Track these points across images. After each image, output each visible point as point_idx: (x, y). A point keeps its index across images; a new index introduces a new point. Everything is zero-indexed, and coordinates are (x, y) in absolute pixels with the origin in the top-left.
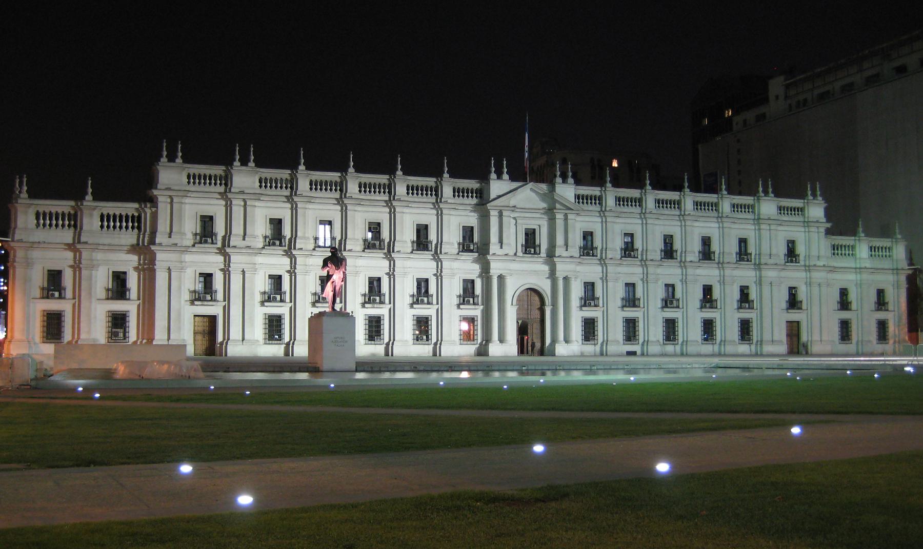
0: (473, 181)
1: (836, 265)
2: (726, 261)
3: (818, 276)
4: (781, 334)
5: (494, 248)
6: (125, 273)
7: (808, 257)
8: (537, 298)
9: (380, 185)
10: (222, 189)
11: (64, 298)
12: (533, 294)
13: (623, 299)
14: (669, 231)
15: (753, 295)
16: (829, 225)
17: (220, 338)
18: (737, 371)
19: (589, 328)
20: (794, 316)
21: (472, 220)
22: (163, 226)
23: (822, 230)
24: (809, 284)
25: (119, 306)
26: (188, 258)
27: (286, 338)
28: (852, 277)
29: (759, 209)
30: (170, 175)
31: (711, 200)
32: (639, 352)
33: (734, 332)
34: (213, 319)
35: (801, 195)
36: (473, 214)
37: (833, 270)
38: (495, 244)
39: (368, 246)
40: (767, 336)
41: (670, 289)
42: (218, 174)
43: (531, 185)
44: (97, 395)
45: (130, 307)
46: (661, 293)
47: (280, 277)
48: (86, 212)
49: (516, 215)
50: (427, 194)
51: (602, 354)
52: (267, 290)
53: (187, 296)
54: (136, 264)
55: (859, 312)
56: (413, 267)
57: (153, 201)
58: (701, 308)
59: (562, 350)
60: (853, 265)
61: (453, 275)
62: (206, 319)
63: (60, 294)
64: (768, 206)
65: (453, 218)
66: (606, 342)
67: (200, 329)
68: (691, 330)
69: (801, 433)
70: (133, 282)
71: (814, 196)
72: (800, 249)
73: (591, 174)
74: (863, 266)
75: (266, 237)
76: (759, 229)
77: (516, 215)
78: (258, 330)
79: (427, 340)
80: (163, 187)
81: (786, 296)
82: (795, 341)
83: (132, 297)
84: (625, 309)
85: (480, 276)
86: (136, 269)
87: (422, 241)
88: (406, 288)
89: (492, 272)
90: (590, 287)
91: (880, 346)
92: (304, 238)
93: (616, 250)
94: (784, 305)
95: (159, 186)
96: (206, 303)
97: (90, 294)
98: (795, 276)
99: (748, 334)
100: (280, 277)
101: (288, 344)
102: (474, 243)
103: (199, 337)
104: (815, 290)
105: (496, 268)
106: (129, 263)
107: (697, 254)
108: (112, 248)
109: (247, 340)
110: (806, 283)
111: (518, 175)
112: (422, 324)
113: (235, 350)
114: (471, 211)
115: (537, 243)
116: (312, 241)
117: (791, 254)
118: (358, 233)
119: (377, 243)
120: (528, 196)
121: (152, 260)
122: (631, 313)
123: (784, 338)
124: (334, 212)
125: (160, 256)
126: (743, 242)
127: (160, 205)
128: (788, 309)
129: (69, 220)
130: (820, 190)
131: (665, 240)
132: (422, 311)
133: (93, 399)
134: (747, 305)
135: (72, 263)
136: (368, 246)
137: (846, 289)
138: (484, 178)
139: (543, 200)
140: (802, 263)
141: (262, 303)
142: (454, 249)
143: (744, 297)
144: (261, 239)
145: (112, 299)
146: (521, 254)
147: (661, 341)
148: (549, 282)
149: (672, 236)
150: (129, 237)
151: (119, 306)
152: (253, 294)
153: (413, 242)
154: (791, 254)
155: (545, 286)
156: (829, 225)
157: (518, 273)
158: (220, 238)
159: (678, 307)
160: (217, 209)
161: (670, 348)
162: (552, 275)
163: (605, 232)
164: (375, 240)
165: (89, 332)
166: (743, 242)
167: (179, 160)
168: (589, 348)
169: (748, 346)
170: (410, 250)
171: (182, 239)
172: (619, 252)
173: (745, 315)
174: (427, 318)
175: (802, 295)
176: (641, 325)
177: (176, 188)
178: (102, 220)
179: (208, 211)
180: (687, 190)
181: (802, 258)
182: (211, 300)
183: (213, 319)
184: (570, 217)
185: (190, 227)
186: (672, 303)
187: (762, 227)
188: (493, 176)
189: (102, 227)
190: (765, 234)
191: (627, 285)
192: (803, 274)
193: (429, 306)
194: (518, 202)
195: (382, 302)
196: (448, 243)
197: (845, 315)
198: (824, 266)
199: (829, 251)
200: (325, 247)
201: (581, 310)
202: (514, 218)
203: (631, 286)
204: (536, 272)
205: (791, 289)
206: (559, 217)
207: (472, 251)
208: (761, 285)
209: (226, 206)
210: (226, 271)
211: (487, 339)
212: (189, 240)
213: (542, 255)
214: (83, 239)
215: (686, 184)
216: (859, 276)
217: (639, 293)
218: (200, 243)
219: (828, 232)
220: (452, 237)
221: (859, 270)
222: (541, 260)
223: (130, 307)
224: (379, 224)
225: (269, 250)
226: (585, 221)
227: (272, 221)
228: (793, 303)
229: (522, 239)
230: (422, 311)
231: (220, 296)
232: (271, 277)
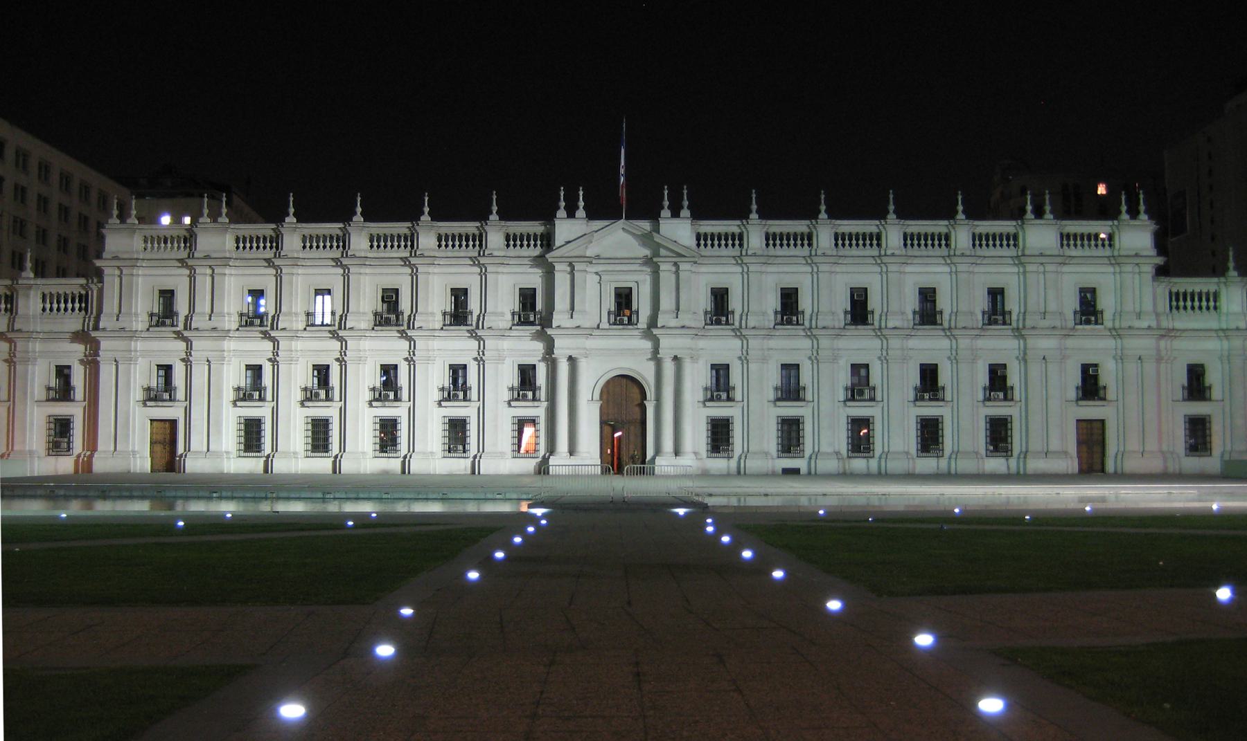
0: (537, 223)
1: (1178, 325)
2: (820, 324)
3: (1140, 345)
5: (559, 318)
6: (69, 367)
7: (1119, 314)
8: (636, 390)
9: (399, 236)
10: (337, 254)
11: (733, 400)
12: (630, 383)
13: (776, 389)
14: (859, 281)
15: (1014, 379)
16: (1160, 261)
17: (180, 449)
19: (720, 434)
20: (1092, 411)
21: (534, 279)
22: (110, 305)
23: (1148, 269)
24: (1121, 358)
25: (62, 409)
26: (139, 345)
27: (267, 448)
28: (1213, 345)
29: (1024, 240)
30: (119, 241)
31: (936, 230)
32: (804, 470)
34: (173, 423)
35: (1018, 214)
36: (644, 268)
37: (1169, 333)
38: (561, 312)
39: (381, 321)
40: (1036, 444)
41: (793, 373)
42: (470, 233)
43: (621, 223)
44: (351, 523)
45: (75, 411)
46: (773, 377)
47: (260, 367)
48: (21, 293)
49: (600, 268)
50: (1082, 246)
52: (243, 385)
53: (139, 395)
54: (81, 356)
55: (1227, 402)
56: (441, 350)
57: (99, 274)
58: (916, 400)
59: (665, 464)
60: (1215, 325)
61: (500, 359)
62: (167, 425)
63: (396, 395)
64: (1041, 235)
65: (503, 279)
66: (746, 454)
67: (160, 437)
68: (827, 433)
69: (1231, 600)
70: (78, 379)
71: (1134, 214)
72: (1106, 302)
73: (716, 200)
74: (1233, 326)
75: (151, 315)
76: (1025, 272)
77: (600, 268)
78: (229, 437)
79: (464, 452)
80: (109, 256)
83: (1213, 397)
84: (778, 403)
85: (544, 359)
86: (82, 362)
87: (459, 315)
88: (433, 378)
89: (557, 352)
90: (721, 372)
91: (52, 460)
92: (290, 314)
93: (764, 314)
95: (105, 255)
96: (160, 404)
97: (25, 393)
98: (1093, 346)
99: (1005, 440)
100: (260, 367)
101: (336, 457)
102: (532, 311)
103: (158, 448)
104: (1035, 370)
105: (563, 347)
106: (73, 354)
107: (911, 316)
108: (52, 336)
109: (215, 449)
110: (1114, 358)
111: (603, 209)
112: (457, 429)
113: (194, 465)
114: (532, 266)
115: (634, 307)
116: (304, 318)
117: (1088, 309)
118: (367, 302)
119: (393, 317)
120: (619, 238)
121: (96, 353)
122: (790, 410)
123: (1072, 448)
124: (333, 278)
125: (104, 345)
126: (996, 294)
127: (106, 279)
128: (1078, 400)
129: (80, 302)
130: (1051, 204)
132: (456, 410)
133: (345, 527)
134: (1001, 395)
135: (7, 356)
136: (381, 321)
138: (548, 217)
139: (644, 245)
140: (1108, 324)
141: (234, 403)
142: (506, 320)
143: (998, 380)
144: (236, 318)
145: (54, 400)
146: (607, 326)
147: (844, 452)
148: (652, 365)
150: (74, 322)
151: (62, 409)
152: (220, 391)
153: (846, 312)
154: (1088, 309)
155: (645, 372)
156: (1160, 261)
157: (598, 356)
158: (181, 319)
159: (872, 399)
160: (178, 281)
161: (859, 464)
162: (656, 357)
163: (746, 286)
164: (390, 312)
165: (24, 442)
166: (996, 294)
167: (1049, 216)
168: (719, 464)
169: (1002, 461)
170: (438, 325)
171: (291, 322)
172: (772, 317)
173: (999, 410)
174: (259, 420)
175: (1107, 376)
176: (808, 428)
177: (125, 256)
179: (168, 284)
180: (892, 216)
181: (1107, 316)
182: (170, 400)
183: (173, 423)
184: (683, 267)
185: (143, 304)
186: (861, 393)
187: (1029, 268)
188: (562, 213)
190: (203, 283)
191: (784, 366)
192: (1111, 343)
194: (597, 249)
195: (397, 399)
196: (494, 314)
197: (1198, 408)
198: (1149, 328)
199: (1163, 304)
200: (322, 325)
201: (145, 405)
202: (597, 273)
203: (791, 370)
204: (632, 352)
205: (1085, 368)
206: (666, 268)
207: (532, 324)
208: (1025, 361)
209: (190, 276)
210: (187, 361)
211: (551, 449)
212: (141, 323)
213: (639, 326)
214: (17, 327)
215: (892, 208)
216: (1226, 344)
217: (806, 378)
218: (157, 326)
219: (1162, 272)
220: (503, 302)
221: (1224, 333)
222: (636, 333)
223: (75, 411)
224: (396, 291)
225: (244, 332)
226: (718, 270)
228: (1090, 386)
229: (610, 303)
230: (456, 410)
231: (542, 394)
232: (248, 367)
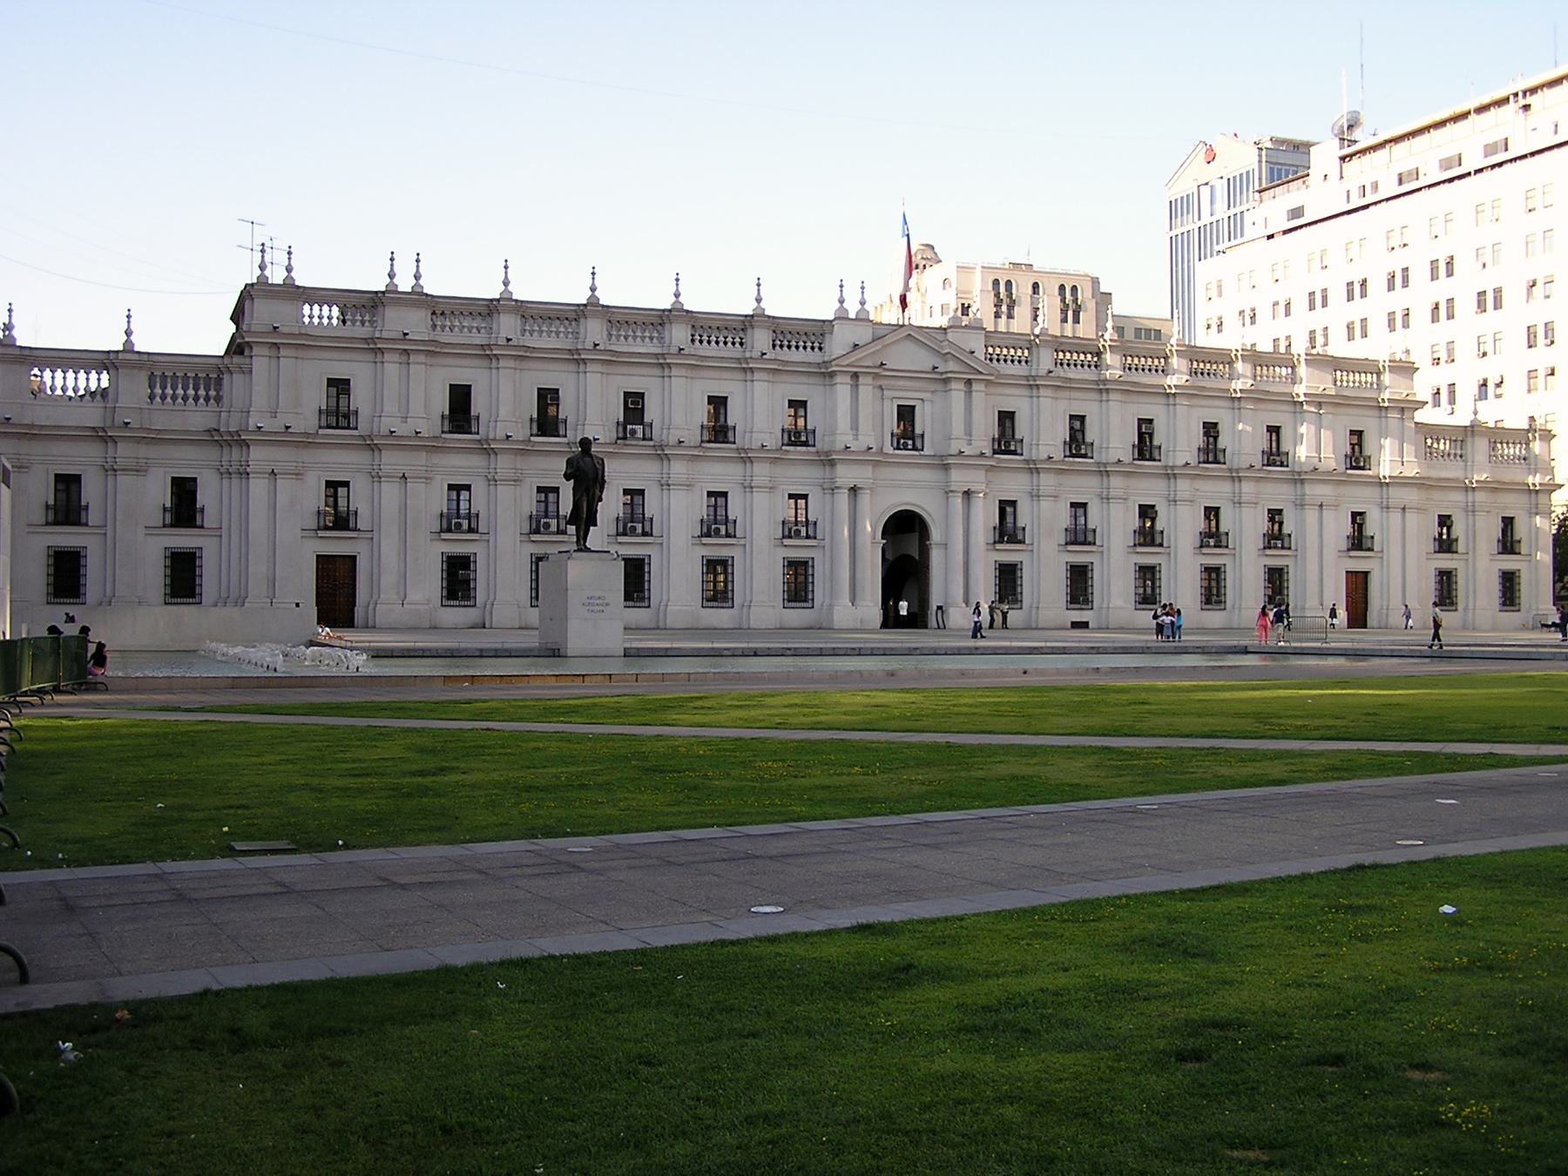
4: (1337, 594)
18: (1341, 661)
33: (1491, 589)
51: (1464, 628)
81: (1347, 528)
82: (337, 594)
94: (1344, 544)
115: (918, 431)
131: (1139, 428)
137: (1512, 518)
145: (56, 523)
146: (891, 451)
149: (1150, 421)
178: (152, 386)
189: (152, 397)
193: (728, 541)
227: (711, 400)
228: (1359, 541)
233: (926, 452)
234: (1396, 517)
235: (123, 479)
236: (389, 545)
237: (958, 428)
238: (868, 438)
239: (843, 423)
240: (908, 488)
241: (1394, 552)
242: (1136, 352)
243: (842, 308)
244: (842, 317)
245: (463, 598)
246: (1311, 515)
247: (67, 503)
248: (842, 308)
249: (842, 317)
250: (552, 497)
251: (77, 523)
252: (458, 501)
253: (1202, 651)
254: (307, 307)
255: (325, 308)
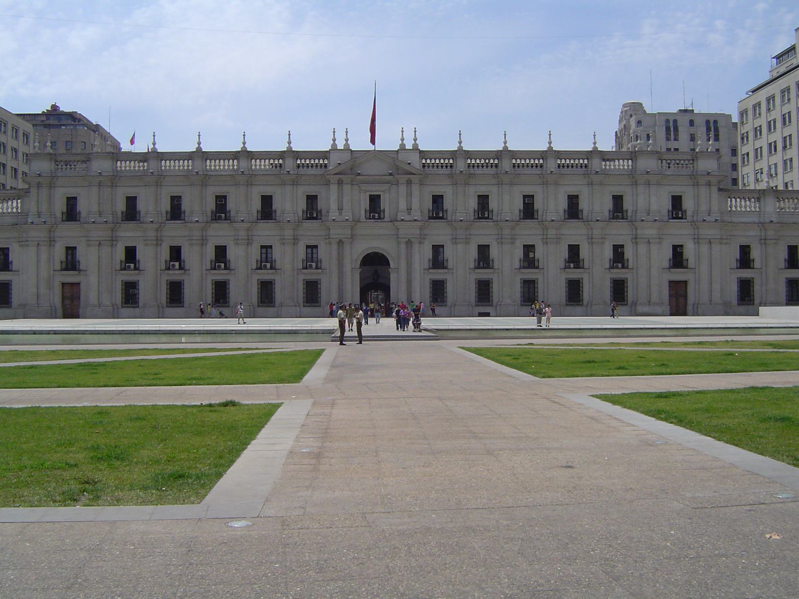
131: (524, 201)
145: (740, 268)
233: (386, 220)
234: (704, 248)
235: (35, 249)
236: (93, 279)
237: (403, 206)
238: (416, 215)
239: (334, 206)
240: (374, 239)
241: (704, 268)
242: (431, 156)
243: (334, 145)
244: (334, 147)
245: (132, 303)
246: (642, 249)
247: (745, 260)
248: (334, 145)
249: (334, 147)
250: (269, 250)
251: (749, 267)
252: (312, 253)
253: (426, 330)
254: (208, 161)
255: (226, 161)
